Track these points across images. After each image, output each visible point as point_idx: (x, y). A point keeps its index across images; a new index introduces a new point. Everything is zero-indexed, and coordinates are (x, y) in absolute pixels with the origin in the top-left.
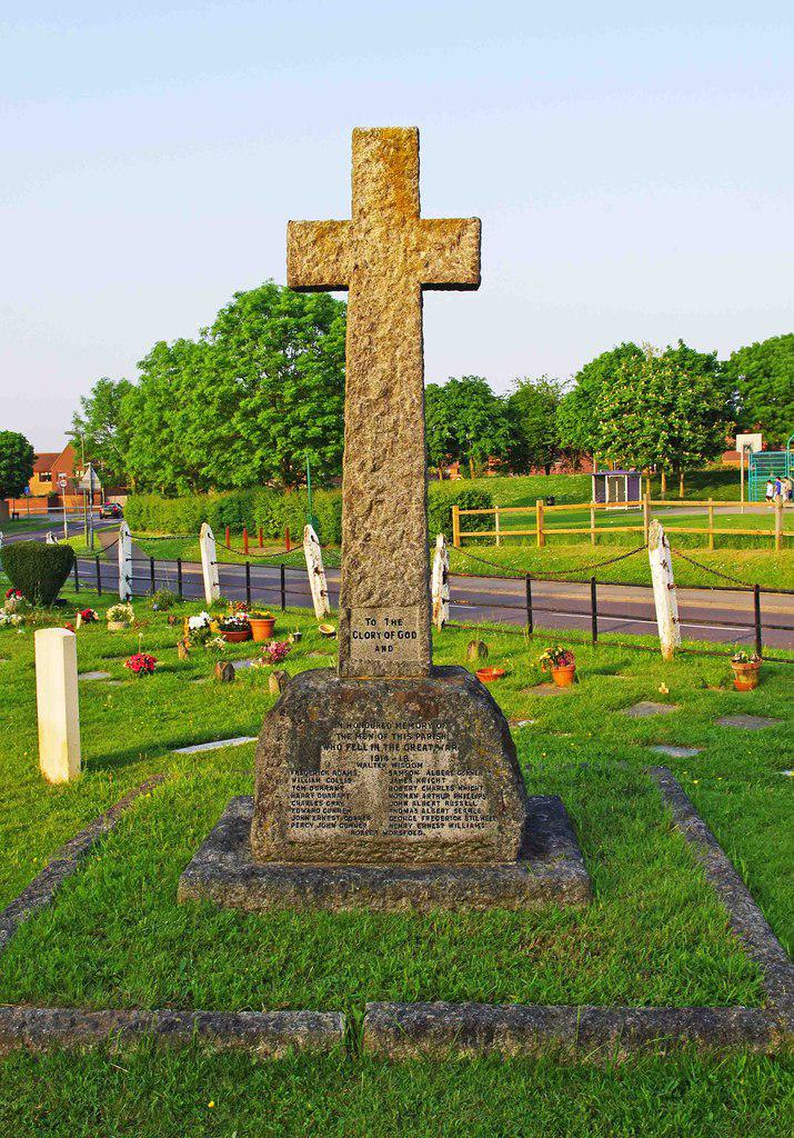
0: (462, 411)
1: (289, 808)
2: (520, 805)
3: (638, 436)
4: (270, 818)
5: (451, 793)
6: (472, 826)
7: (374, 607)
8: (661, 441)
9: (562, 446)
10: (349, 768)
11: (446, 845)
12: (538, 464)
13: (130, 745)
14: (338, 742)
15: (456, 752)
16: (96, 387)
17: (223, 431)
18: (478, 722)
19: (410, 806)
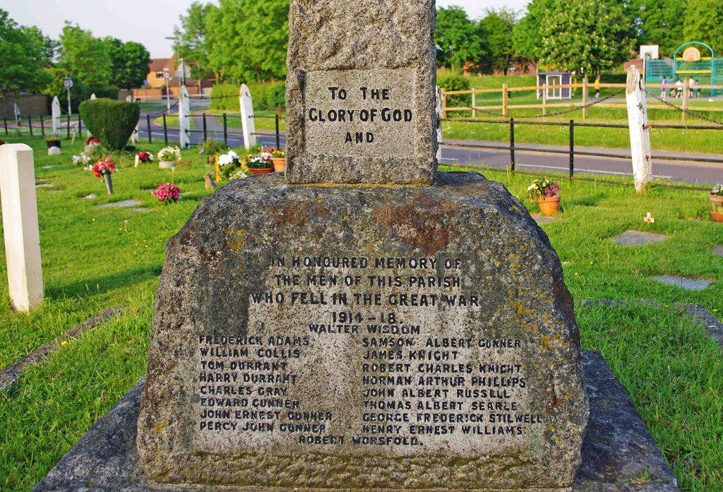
0: (447, 30)
1: (196, 399)
2: (582, 396)
3: (570, 48)
4: (166, 413)
5: (468, 377)
6: (501, 431)
7: (342, 68)
8: (585, 51)
9: (516, 55)
10: (297, 332)
11: (456, 460)
12: (499, 68)
13: (119, 269)
14: (277, 290)
15: (476, 308)
16: (190, 8)
17: (277, 35)
18: (514, 259)
19: (398, 397)
